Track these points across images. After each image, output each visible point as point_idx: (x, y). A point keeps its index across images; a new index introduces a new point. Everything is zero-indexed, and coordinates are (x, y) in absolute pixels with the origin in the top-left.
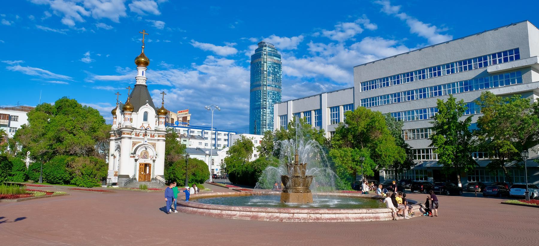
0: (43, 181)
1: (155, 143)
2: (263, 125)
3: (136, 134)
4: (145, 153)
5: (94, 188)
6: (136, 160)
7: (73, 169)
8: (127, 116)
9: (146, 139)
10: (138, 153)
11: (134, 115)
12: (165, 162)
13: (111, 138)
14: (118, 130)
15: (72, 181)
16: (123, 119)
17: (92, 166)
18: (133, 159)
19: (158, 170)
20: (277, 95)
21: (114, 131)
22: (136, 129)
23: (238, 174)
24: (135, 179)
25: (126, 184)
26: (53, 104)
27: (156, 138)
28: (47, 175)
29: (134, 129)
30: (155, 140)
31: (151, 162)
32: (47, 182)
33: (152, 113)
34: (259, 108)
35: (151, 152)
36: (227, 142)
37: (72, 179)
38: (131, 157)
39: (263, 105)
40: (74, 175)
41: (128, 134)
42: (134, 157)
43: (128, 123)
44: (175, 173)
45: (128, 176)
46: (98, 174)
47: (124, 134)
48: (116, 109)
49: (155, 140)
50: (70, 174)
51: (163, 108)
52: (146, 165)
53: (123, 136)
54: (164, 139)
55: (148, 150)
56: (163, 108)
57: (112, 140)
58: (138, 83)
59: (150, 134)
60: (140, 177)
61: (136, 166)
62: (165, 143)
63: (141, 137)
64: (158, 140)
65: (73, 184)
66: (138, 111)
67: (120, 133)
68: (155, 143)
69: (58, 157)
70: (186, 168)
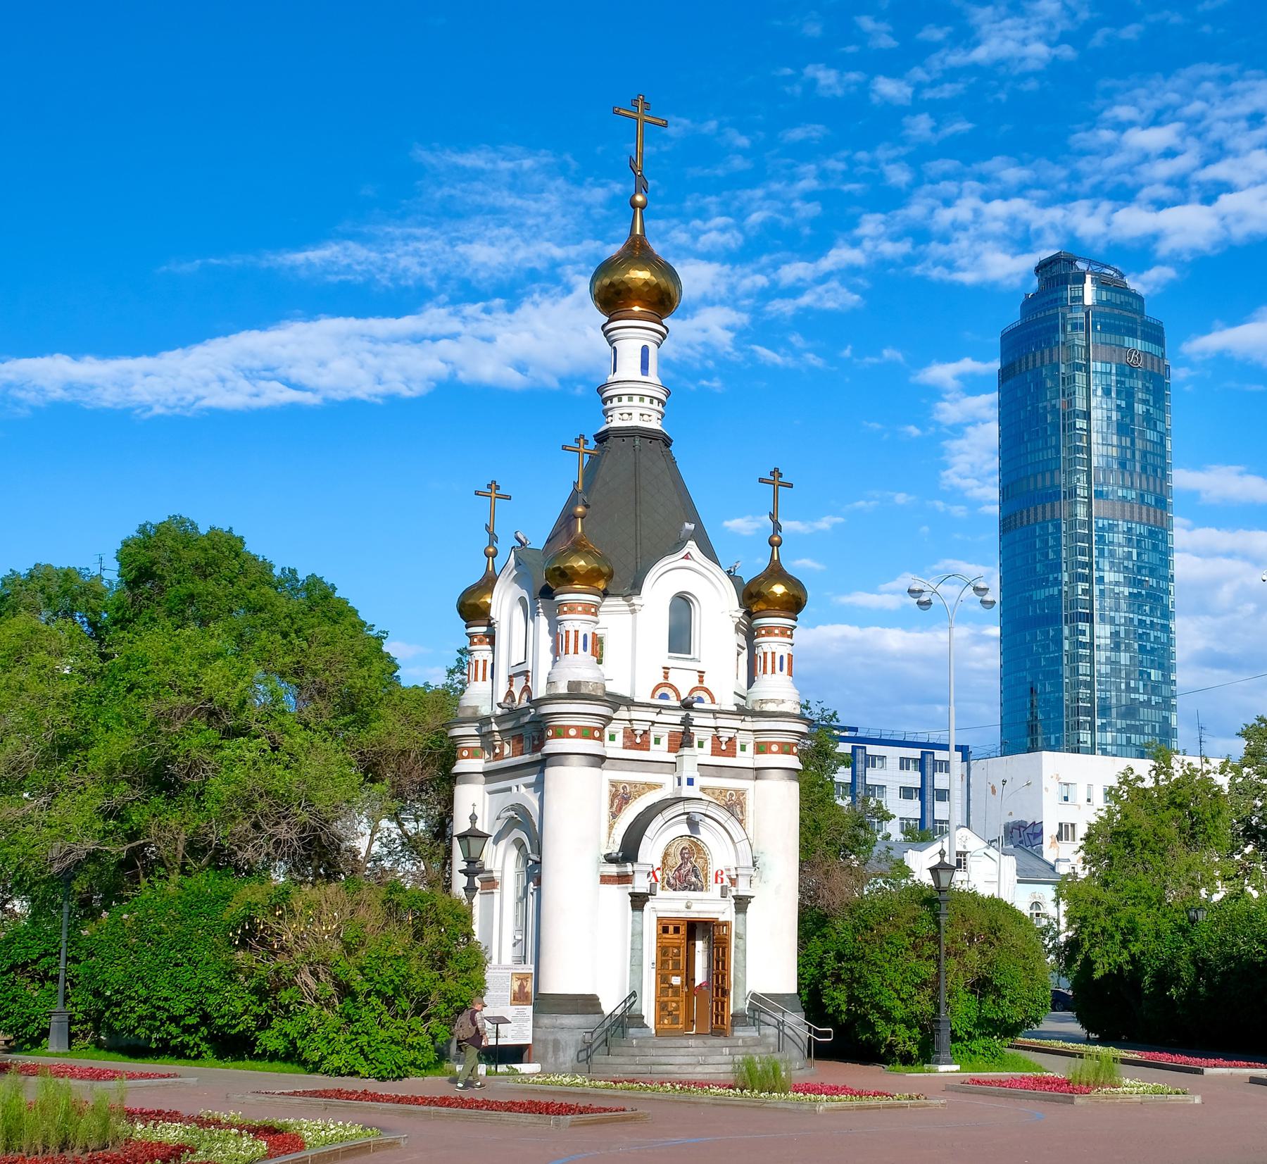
0: (72, 1036)
1: (741, 793)
2: (1077, 711)
3: (630, 734)
4: (686, 855)
5: (416, 1084)
6: (638, 901)
7: (282, 960)
8: (575, 624)
9: (689, 770)
10: (651, 851)
11: (613, 619)
12: (801, 921)
13: (461, 766)
14: (512, 713)
15: (270, 1040)
16: (546, 641)
17: (400, 940)
18: (618, 896)
19: (769, 961)
20: (1148, 543)
21: (485, 721)
22: (630, 703)
23: (1164, 978)
24: (638, 1020)
25: (586, 1054)
26: (203, 530)
27: (746, 758)
28: (109, 1004)
29: (617, 702)
30: (737, 771)
31: (723, 911)
32: (99, 1045)
33: (718, 609)
34: (1053, 619)
35: (720, 852)
36: (916, 803)
37: (264, 1022)
38: (605, 879)
39: (1074, 603)
40: (284, 996)
41: (586, 733)
42: (624, 879)
43: (579, 668)
44: (857, 980)
45: (588, 1004)
46: (421, 983)
47: (562, 733)
48: (488, 583)
49: (737, 771)
50: (261, 993)
51: (776, 572)
52: (696, 928)
53: (553, 746)
54: (793, 762)
55: (704, 835)
56: (776, 572)
57: (466, 776)
58: (616, 423)
59: (707, 736)
60: (662, 1007)
61: (637, 935)
62: (795, 786)
63: (660, 752)
64: (758, 772)
65: (273, 1056)
66: (636, 588)
67: (529, 734)
68: (741, 793)
69: (159, 894)
70: (932, 944)
